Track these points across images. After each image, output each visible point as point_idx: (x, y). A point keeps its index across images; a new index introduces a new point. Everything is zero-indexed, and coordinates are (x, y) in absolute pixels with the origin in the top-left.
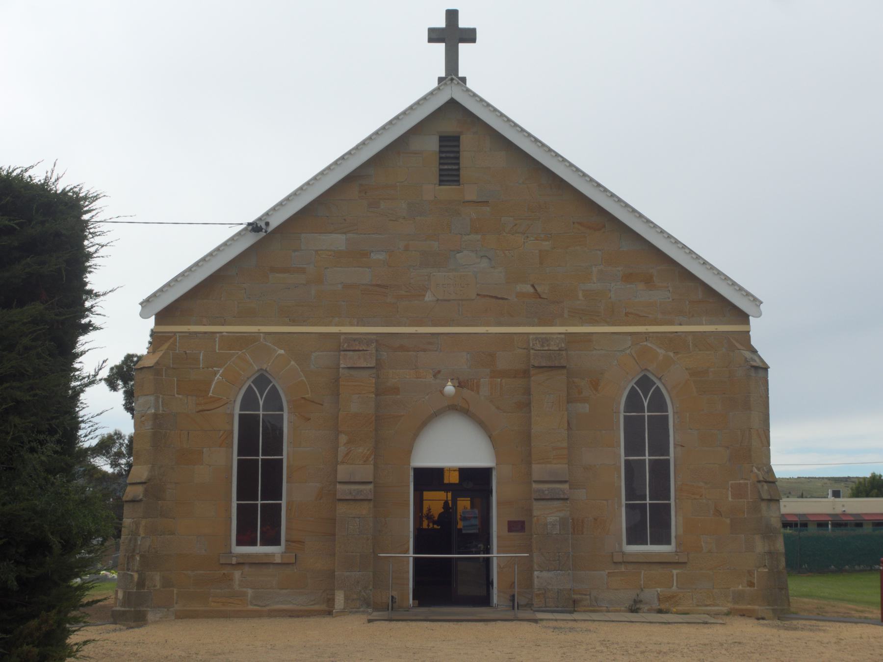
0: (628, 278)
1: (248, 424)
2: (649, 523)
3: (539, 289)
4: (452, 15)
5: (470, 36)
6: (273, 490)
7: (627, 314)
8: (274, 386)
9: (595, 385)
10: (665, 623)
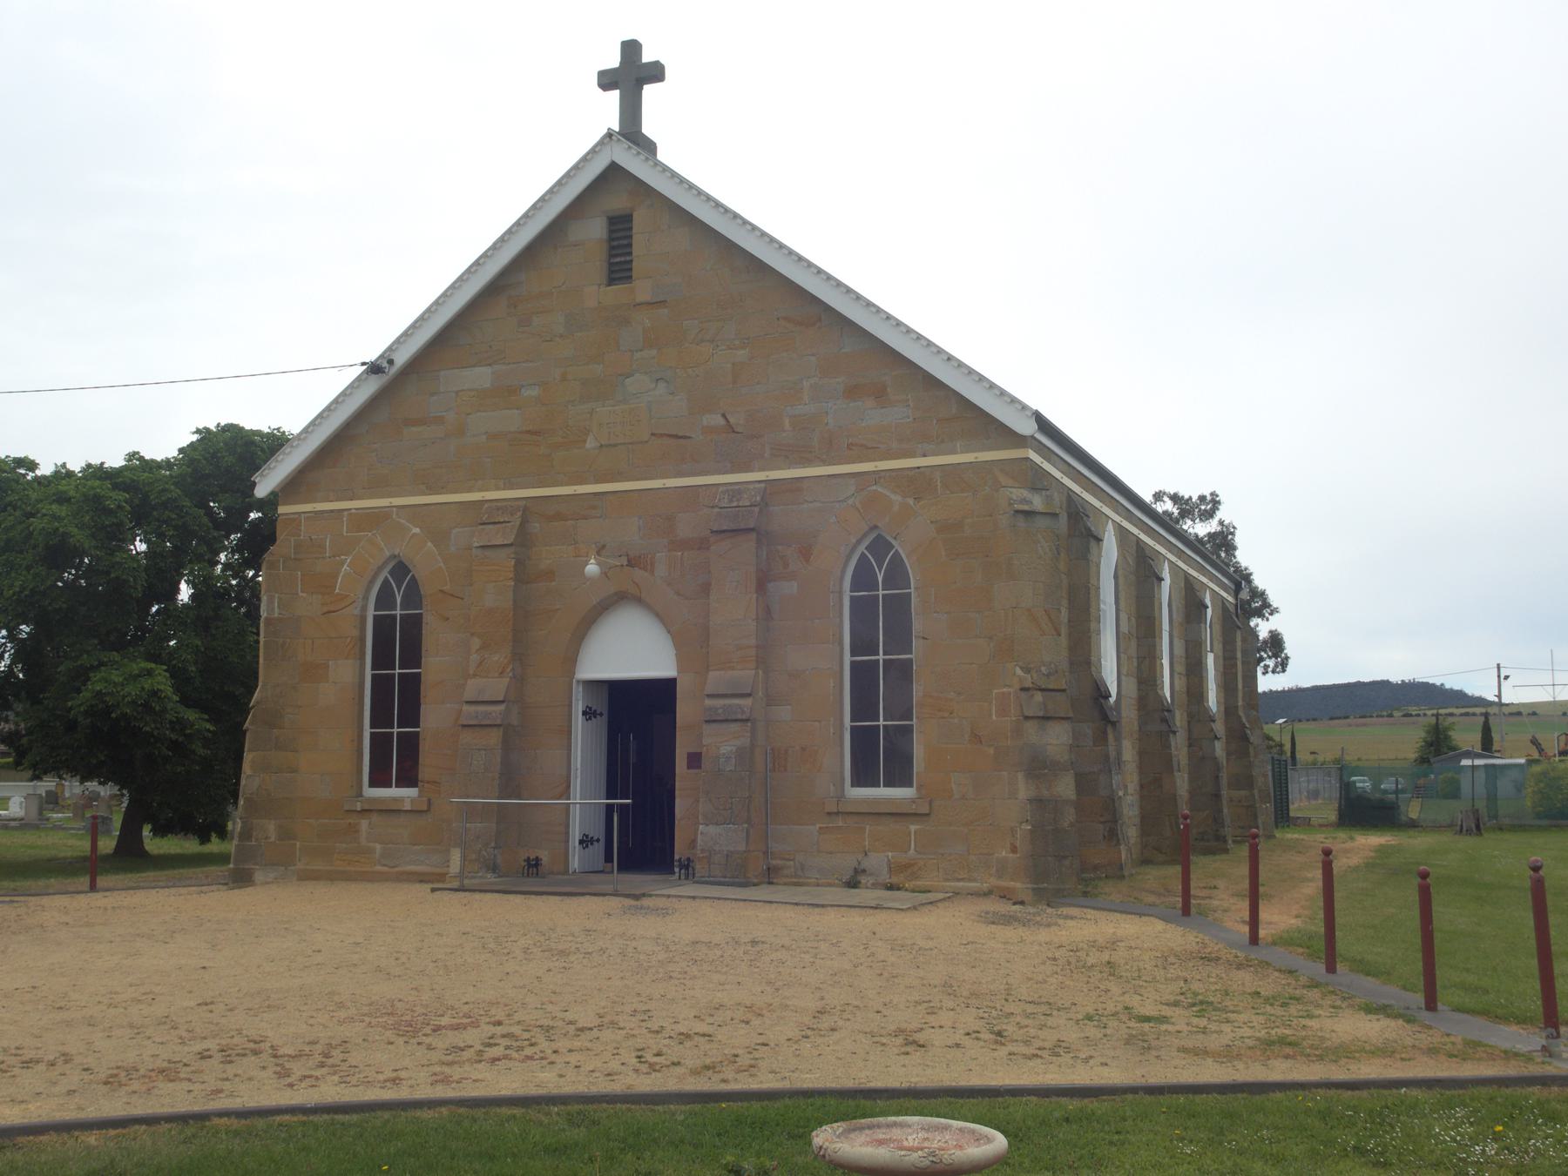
0: (852, 392)
1: (383, 627)
2: (879, 756)
3: (732, 420)
4: (631, 49)
5: (656, 73)
6: (411, 714)
7: (849, 446)
8: (897, 554)
9: (806, 554)
10: (817, 906)
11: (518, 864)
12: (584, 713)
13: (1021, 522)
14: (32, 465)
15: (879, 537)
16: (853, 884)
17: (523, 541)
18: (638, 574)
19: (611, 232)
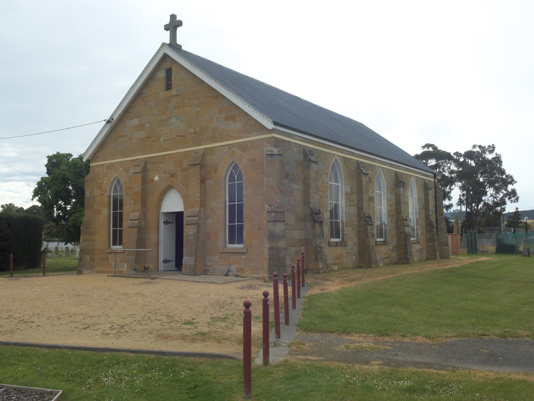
0: (227, 119)
2: (236, 234)
4: (173, 17)
5: (180, 24)
7: (226, 136)
9: (215, 171)
11: (142, 269)
12: (164, 222)
13: (269, 158)
14: (71, 155)
15: (236, 164)
16: (227, 275)
17: (145, 170)
18: (174, 179)
19: (168, 74)
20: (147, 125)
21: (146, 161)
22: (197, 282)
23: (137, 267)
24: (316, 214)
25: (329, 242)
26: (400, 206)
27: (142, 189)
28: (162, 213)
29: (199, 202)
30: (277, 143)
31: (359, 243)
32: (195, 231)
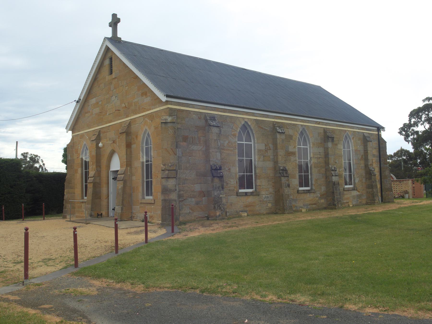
4: (114, 16)
13: (163, 125)
20: (100, 103)
21: (100, 131)
22: (109, 227)
23: (93, 214)
24: (216, 169)
25: (237, 193)
26: (328, 158)
27: (96, 153)
28: (111, 171)
29: (125, 163)
30: (171, 112)
31: (275, 192)
32: (122, 186)
